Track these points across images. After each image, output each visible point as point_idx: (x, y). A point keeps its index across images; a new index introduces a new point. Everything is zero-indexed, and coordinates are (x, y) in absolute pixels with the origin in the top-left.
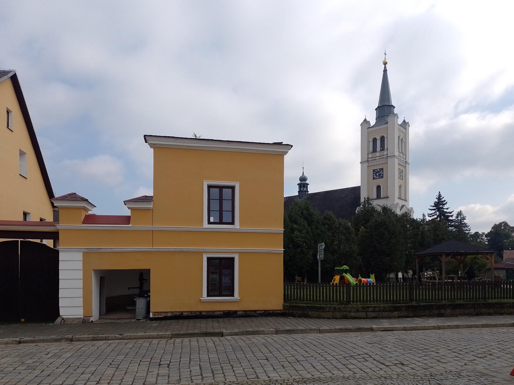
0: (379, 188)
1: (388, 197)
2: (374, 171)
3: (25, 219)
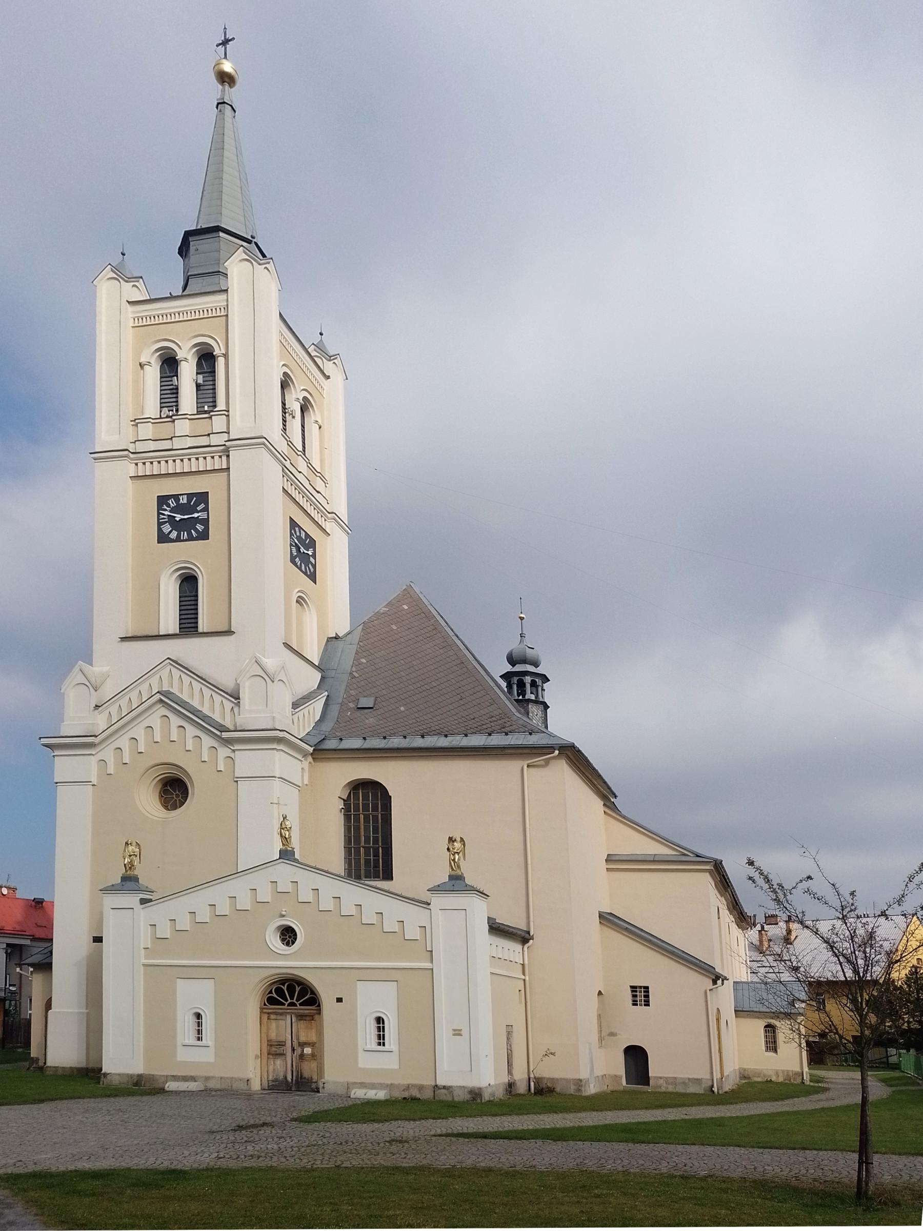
0: (189, 582)
1: (229, 632)
2: (162, 500)
3: (348, 831)
